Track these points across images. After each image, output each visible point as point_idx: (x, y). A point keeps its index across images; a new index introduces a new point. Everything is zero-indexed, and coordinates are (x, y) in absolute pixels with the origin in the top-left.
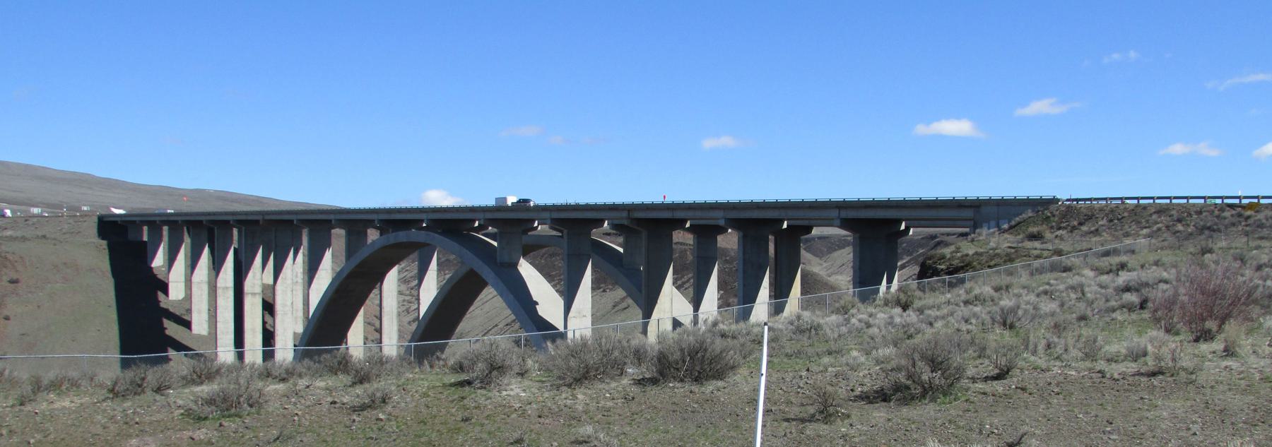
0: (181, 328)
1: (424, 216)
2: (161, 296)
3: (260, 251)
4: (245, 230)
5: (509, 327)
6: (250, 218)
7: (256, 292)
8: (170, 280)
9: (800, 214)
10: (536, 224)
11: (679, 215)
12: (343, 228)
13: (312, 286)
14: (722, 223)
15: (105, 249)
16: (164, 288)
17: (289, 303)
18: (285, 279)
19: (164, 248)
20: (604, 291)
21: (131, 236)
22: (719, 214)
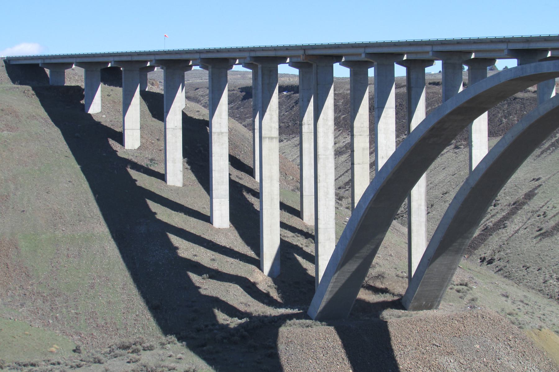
6: (136, 58)
7: (273, 136)
8: (126, 126)
9: (419, 49)
10: (191, 63)
11: (280, 54)
14: (430, 56)
15: (33, 95)
16: (120, 137)
18: (327, 120)
20: (457, 147)
22: (428, 48)
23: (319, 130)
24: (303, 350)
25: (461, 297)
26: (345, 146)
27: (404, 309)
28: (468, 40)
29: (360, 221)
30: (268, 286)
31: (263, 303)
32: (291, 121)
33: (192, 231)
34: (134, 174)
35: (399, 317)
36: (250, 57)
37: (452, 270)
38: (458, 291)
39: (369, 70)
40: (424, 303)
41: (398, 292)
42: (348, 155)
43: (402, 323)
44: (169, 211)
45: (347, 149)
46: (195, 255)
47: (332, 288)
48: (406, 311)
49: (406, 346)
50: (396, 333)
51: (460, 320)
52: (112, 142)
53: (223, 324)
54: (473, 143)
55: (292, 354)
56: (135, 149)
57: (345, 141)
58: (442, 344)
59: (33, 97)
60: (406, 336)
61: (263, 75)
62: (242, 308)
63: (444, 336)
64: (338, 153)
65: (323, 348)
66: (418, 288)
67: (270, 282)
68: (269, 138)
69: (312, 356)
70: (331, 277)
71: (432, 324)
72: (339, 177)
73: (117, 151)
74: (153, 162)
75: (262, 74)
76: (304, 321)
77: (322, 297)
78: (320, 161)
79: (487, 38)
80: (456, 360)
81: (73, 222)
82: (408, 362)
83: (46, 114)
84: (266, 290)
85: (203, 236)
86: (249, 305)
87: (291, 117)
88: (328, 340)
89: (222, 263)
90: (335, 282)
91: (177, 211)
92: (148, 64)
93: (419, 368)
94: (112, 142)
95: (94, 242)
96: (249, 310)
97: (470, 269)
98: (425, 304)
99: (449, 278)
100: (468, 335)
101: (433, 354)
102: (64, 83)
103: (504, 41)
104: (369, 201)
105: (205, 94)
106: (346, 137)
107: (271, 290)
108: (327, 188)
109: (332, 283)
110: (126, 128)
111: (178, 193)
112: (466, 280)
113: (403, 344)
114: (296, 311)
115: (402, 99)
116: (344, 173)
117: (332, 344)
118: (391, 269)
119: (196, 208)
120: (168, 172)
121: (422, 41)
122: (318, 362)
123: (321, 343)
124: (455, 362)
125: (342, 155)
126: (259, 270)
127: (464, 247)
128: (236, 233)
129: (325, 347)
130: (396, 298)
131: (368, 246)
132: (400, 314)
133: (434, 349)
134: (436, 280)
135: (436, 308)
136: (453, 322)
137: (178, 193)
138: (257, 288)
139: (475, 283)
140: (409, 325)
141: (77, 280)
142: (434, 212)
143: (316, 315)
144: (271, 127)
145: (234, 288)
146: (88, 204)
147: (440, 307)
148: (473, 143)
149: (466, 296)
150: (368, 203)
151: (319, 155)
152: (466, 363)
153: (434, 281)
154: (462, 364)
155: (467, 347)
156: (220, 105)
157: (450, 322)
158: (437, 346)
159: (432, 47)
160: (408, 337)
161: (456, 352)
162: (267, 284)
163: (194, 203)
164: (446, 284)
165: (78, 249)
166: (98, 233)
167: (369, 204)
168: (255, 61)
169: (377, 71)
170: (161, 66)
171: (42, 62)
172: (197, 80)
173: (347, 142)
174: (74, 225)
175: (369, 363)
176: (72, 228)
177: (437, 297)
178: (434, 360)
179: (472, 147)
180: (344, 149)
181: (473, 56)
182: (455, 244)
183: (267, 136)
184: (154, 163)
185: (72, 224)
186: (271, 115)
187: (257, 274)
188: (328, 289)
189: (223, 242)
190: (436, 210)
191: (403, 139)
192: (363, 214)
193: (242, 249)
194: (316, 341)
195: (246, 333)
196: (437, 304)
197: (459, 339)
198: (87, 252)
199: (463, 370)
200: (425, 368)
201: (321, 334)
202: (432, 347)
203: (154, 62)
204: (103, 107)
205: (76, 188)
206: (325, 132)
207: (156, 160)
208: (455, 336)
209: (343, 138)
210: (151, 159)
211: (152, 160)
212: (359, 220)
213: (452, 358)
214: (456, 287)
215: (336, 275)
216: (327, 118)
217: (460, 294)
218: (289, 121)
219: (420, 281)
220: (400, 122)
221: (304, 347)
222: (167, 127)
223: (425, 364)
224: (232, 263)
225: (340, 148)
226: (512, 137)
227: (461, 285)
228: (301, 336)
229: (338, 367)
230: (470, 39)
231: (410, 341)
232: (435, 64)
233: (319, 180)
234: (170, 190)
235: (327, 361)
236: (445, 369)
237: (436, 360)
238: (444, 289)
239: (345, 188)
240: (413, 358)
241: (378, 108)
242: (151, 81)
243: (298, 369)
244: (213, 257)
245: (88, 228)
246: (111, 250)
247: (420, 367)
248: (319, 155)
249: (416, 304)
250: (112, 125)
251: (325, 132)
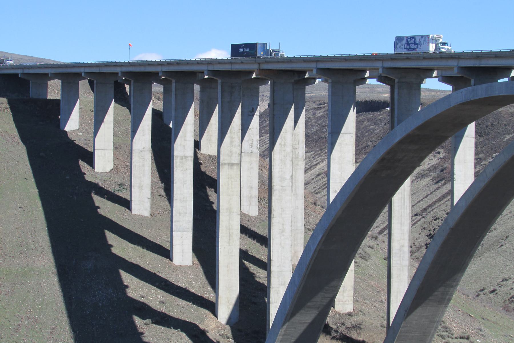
0: (118, 207)
2: (84, 166)
3: (239, 110)
4: (222, 83)
7: (233, 162)
10: (367, 75)
15: (6, 108)
17: (288, 177)
18: (284, 145)
21: (33, 93)
23: (274, 157)
30: (219, 335)
32: (379, 140)
33: (147, 268)
34: (97, 200)
44: (125, 243)
45: (431, 172)
46: (143, 297)
52: (82, 163)
54: (455, 176)
56: (106, 172)
57: (430, 163)
59: (6, 110)
61: (223, 91)
64: (420, 176)
67: (228, 331)
68: (229, 164)
70: (279, 329)
72: (418, 203)
73: (85, 174)
74: (122, 187)
78: (275, 193)
81: (13, 254)
83: (15, 130)
84: (217, 339)
91: (135, 244)
92: (307, 76)
94: (82, 163)
95: (31, 277)
97: (483, 319)
99: (432, 331)
102: (47, 97)
103: (453, 56)
104: (317, 243)
106: (432, 159)
107: (223, 339)
108: (283, 225)
109: (280, 335)
110: (96, 148)
111: (141, 224)
112: (470, 332)
115: (495, 119)
116: (424, 198)
118: (376, 318)
119: (159, 242)
120: (133, 199)
121: (335, 56)
125: (425, 178)
126: (213, 316)
128: (200, 271)
134: (416, 335)
137: (141, 224)
139: (483, 335)
141: (2, 322)
142: (507, 245)
144: (231, 152)
145: (177, 337)
146: (35, 234)
150: (316, 244)
151: (273, 186)
163: (158, 236)
164: (429, 338)
165: (12, 285)
166: (38, 268)
167: (318, 245)
168: (214, 76)
171: (22, 72)
173: (431, 164)
174: (13, 257)
176: (11, 261)
179: (454, 180)
180: (428, 172)
181: (254, 76)
182: (436, 293)
184: (123, 188)
185: (12, 256)
186: (232, 138)
187: (210, 320)
189: (179, 281)
190: (510, 242)
191: (490, 162)
193: (199, 291)
198: (20, 289)
203: (315, 72)
204: (81, 123)
205: (26, 215)
207: (126, 185)
209: (428, 160)
210: (121, 184)
211: (121, 185)
212: (307, 263)
215: (285, 327)
216: (285, 143)
218: (377, 140)
219: (396, 335)
220: (489, 144)
222: (133, 149)
225: (423, 171)
226: (493, 170)
227: (461, 338)
232: (425, 83)
233: (273, 215)
234: (133, 220)
239: (422, 215)
241: (331, 133)
244: (162, 299)
245: (28, 262)
246: (48, 287)
248: (273, 186)
250: (85, 144)
251: (281, 160)
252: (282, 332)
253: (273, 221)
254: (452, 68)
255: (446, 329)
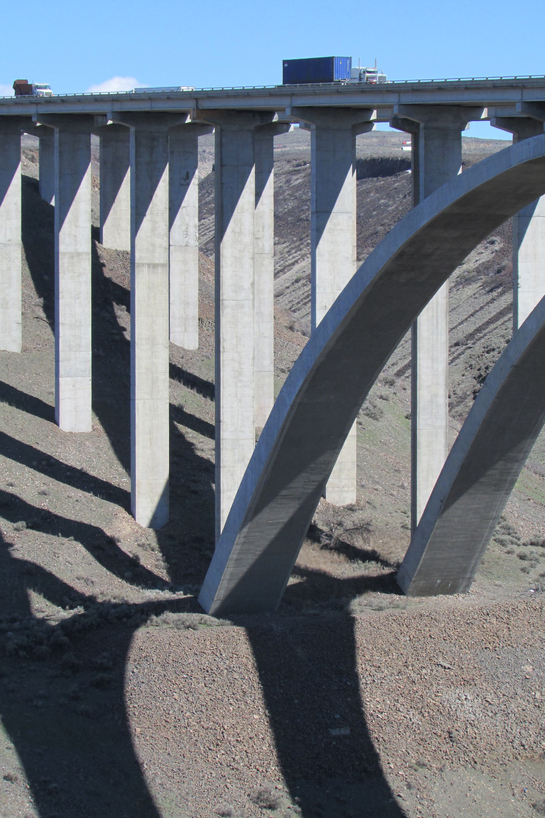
1: (105, 108)
5: (461, 348)
10: (374, 116)
12: (512, 133)
13: (321, 242)
17: (247, 284)
18: (240, 233)
19: (93, 181)
24: (165, 676)
25: (523, 570)
26: (477, 268)
27: (400, 591)
28: (456, 84)
29: (283, 429)
31: (122, 577)
33: (17, 438)
35: (380, 609)
36: (113, 112)
37: (491, 521)
38: (522, 557)
39: (201, 139)
40: (438, 581)
41: (396, 559)
42: (478, 285)
43: (382, 621)
46: (11, 485)
47: (239, 554)
48: (402, 596)
49: (379, 667)
50: (364, 641)
51: (502, 616)
53: (43, 621)
55: (143, 683)
58: (456, 663)
60: (384, 646)
61: (138, 144)
62: (80, 587)
63: (462, 647)
64: (463, 280)
65: (208, 671)
66: (424, 553)
67: (152, 539)
68: (149, 265)
69: (181, 685)
71: (443, 625)
72: (460, 324)
75: (136, 144)
76: (184, 616)
77: (221, 570)
78: (225, 311)
79: (487, 80)
80: (478, 695)
82: (378, 699)
85: (35, 446)
86: (92, 582)
87: (397, 214)
88: (221, 655)
89: (58, 499)
90: (244, 543)
92: (276, 119)
93: (399, 710)
96: (87, 591)
98: (441, 583)
99: (486, 534)
100: (512, 647)
101: (433, 683)
104: (297, 392)
105: (280, 171)
106: (482, 253)
107: (144, 552)
109: (237, 544)
113: (374, 664)
114: (180, 595)
116: (469, 317)
117: (227, 662)
118: (394, 514)
122: (190, 699)
123: (205, 661)
124: (476, 700)
125: (470, 284)
126: (127, 515)
127: (510, 478)
128: (104, 442)
129: (212, 670)
130: (387, 571)
131: (304, 475)
132: (385, 603)
133: (438, 674)
134: (459, 540)
135: (464, 592)
136: (486, 620)
137: (7, 365)
138: (119, 549)
140: (394, 625)
143: (214, 606)
144: (153, 245)
147: (473, 588)
148: (519, 281)
149: (535, 567)
151: (223, 300)
152: (497, 702)
153: (454, 540)
154: (490, 704)
155: (507, 670)
156: (156, 196)
157: (481, 621)
158: (445, 668)
159: (399, 96)
160: (386, 649)
161: (483, 678)
162: (136, 541)
164: (481, 546)
169: (315, 141)
170: (304, 122)
172: (300, 146)
173: (481, 261)
175: (296, 701)
177: (464, 570)
178: (433, 696)
180: (475, 273)
181: (188, 120)
183: (145, 262)
186: (154, 222)
187: (122, 521)
188: (231, 555)
192: (288, 417)
194: (195, 657)
195: (65, 639)
196: (464, 583)
197: (494, 655)
199: (490, 714)
200: (412, 711)
201: (208, 643)
202: (432, 670)
203: (288, 112)
206: (235, 258)
208: (486, 648)
213: (472, 691)
214: (519, 550)
215: (245, 530)
216: (241, 229)
217: (525, 564)
218: (392, 223)
219: (427, 540)
221: (170, 668)
223: (413, 704)
224: (77, 501)
227: (532, 544)
228: (167, 646)
229: (231, 708)
230: (459, 81)
231: (391, 657)
232: (468, 129)
233: (223, 347)
235: (210, 696)
236: (451, 713)
237: (436, 696)
238: (476, 556)
240: (389, 690)
242: (31, 153)
243: (148, 712)
244: (44, 488)
247: (401, 709)
248: (223, 300)
249: (422, 583)
251: (235, 258)
252: (240, 539)
253: (223, 357)
254: (512, 105)
255: (508, 530)
